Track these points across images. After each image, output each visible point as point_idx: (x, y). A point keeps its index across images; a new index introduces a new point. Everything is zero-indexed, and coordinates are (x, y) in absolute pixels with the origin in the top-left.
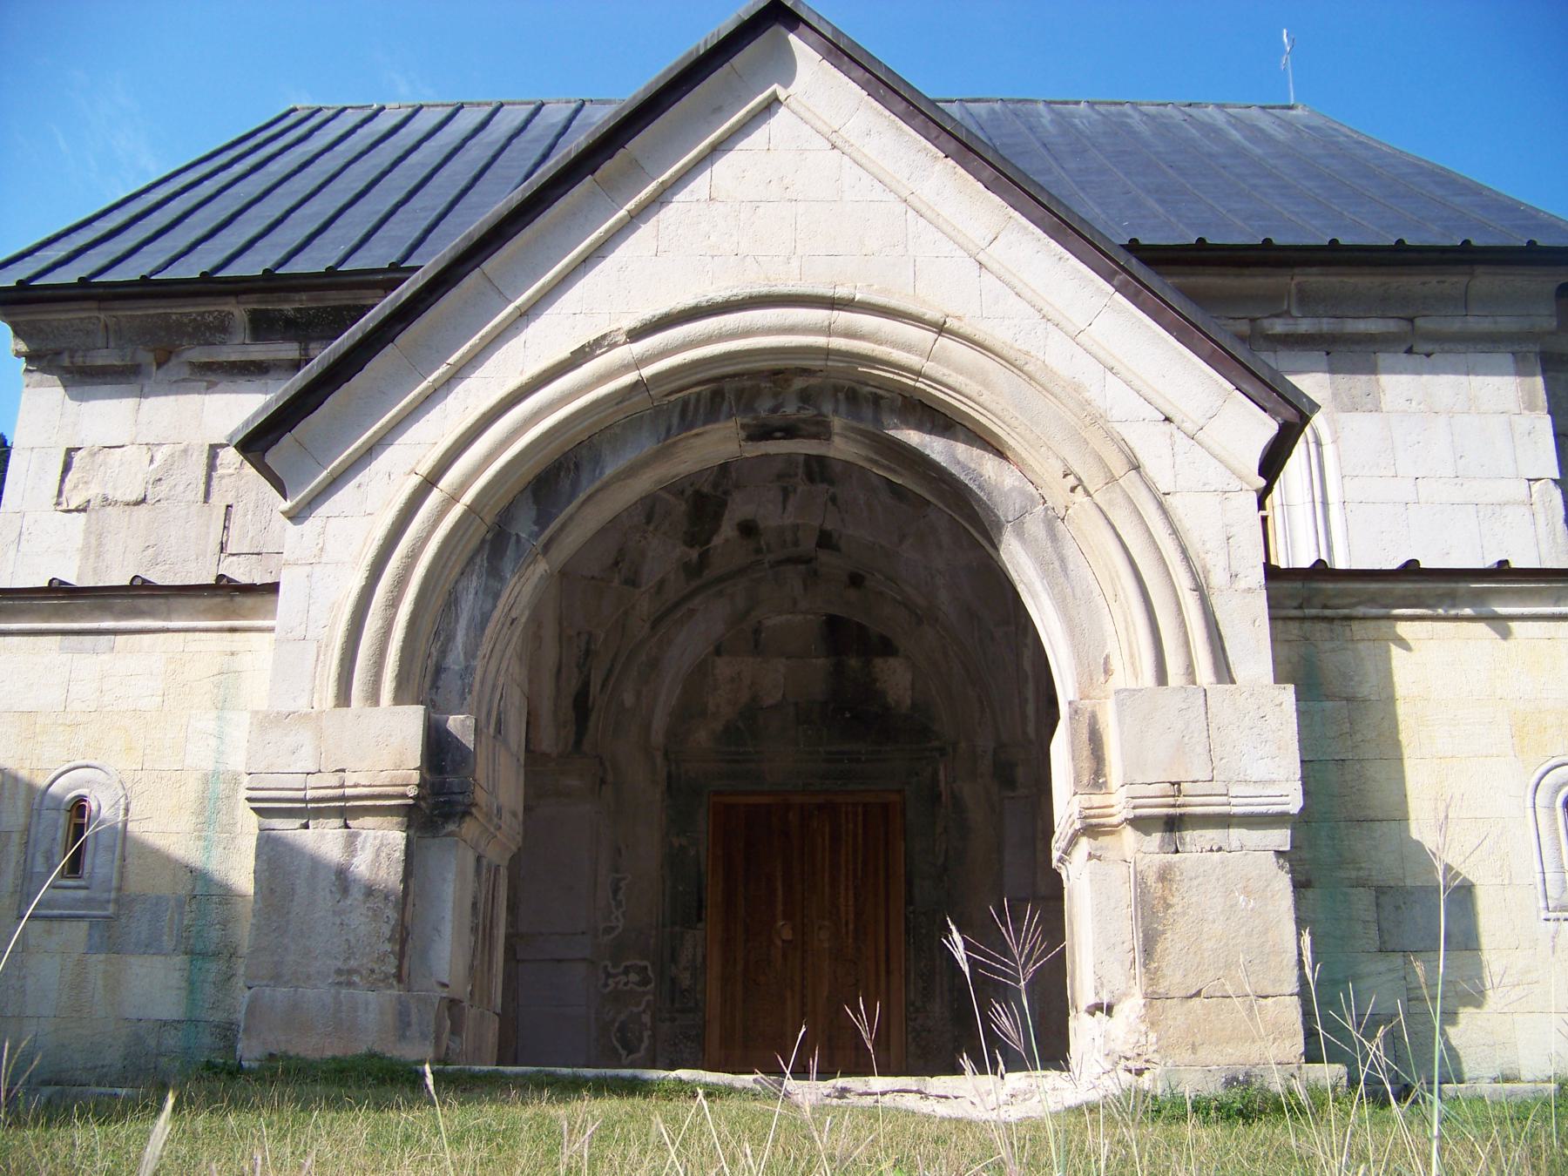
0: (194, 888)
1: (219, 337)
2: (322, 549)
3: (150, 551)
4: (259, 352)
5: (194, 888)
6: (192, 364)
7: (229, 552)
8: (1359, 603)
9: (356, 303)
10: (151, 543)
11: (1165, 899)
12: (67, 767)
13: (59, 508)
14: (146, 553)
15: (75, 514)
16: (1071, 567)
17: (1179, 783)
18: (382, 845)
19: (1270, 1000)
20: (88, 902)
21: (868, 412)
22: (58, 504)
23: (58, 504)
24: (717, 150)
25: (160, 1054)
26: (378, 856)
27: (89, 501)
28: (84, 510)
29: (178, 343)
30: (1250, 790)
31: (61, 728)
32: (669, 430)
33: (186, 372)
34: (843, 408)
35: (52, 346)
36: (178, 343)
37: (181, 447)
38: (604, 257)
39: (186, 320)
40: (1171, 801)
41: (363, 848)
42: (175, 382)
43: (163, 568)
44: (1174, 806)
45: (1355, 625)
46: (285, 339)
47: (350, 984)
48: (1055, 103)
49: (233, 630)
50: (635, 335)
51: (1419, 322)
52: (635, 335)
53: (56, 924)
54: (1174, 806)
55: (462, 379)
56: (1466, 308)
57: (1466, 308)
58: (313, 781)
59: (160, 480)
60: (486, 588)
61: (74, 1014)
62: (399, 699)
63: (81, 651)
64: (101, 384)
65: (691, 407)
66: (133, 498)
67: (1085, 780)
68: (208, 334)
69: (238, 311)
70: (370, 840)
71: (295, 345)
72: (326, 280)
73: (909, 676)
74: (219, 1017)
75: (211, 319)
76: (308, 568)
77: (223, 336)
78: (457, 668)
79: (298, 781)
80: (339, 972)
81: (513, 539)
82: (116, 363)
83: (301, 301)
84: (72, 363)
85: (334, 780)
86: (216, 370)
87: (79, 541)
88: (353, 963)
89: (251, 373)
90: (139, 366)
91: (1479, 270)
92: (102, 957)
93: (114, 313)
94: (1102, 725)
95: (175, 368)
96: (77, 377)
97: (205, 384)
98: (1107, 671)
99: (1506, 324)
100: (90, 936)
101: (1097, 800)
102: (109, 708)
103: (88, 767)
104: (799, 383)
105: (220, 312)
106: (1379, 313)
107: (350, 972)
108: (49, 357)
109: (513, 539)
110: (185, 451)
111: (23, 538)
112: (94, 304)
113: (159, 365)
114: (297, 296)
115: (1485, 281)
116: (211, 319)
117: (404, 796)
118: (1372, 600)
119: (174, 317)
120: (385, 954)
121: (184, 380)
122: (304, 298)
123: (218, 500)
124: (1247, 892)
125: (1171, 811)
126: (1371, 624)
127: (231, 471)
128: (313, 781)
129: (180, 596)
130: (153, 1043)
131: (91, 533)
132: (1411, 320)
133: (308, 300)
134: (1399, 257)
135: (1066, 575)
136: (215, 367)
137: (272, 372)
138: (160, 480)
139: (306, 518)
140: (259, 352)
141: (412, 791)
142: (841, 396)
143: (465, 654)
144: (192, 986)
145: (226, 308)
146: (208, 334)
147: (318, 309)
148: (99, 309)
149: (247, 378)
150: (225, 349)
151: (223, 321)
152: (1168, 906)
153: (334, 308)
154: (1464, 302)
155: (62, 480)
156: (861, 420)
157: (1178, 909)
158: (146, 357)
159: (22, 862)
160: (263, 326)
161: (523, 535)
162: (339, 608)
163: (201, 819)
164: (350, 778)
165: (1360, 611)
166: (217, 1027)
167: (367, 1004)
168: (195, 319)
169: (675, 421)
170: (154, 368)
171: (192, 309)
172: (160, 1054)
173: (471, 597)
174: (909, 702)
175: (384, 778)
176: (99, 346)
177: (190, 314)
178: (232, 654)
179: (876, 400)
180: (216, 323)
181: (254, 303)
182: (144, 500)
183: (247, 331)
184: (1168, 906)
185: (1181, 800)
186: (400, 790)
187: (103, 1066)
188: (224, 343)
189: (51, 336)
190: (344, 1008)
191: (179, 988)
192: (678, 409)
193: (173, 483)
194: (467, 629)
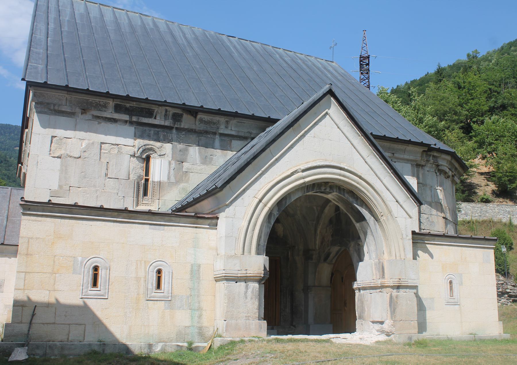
0: (191, 293)
1: (104, 109)
2: (235, 214)
3: (83, 174)
4: (116, 116)
5: (191, 293)
6: (93, 115)
7: (108, 177)
8: (419, 240)
9: (150, 108)
10: (84, 171)
11: (397, 302)
12: (155, 261)
13: (50, 155)
14: (81, 174)
15: (56, 158)
16: (378, 231)
17: (400, 279)
18: (254, 287)
19: (412, 322)
20: (164, 297)
21: (342, 192)
22: (50, 154)
23: (50, 154)
24: (316, 124)
25: (185, 334)
26: (253, 290)
27: (62, 155)
28: (60, 158)
29: (90, 108)
30: (411, 281)
31: (152, 250)
32: (304, 192)
33: (90, 117)
34: (338, 191)
35: (47, 101)
36: (90, 108)
37: (91, 142)
38: (293, 148)
39: (94, 102)
40: (399, 282)
41: (250, 288)
42: (87, 120)
43: (88, 179)
44: (399, 283)
45: (418, 244)
46: (125, 114)
47: (249, 319)
48: (286, 50)
49: (196, 227)
50: (303, 171)
51: (395, 155)
52: (303, 171)
53: (156, 302)
54: (399, 283)
55: (264, 174)
56: (405, 153)
57: (405, 153)
58: (240, 272)
59: (85, 151)
60: (268, 226)
61: (162, 325)
62: (258, 253)
63: (155, 229)
64: (62, 116)
65: (309, 187)
66: (77, 156)
67: (381, 277)
68: (100, 108)
69: (111, 103)
70: (251, 286)
71: (128, 116)
72: (144, 101)
73: (283, 228)
74: (199, 325)
75: (102, 103)
76: (232, 219)
77: (105, 109)
78: (262, 245)
79: (236, 272)
80: (246, 317)
81: (273, 215)
82: (69, 111)
83: (133, 104)
84: (54, 108)
85: (245, 272)
86: (100, 118)
87: (59, 167)
88: (249, 315)
89: (112, 121)
90: (75, 113)
91: (410, 145)
92: (168, 310)
93: (71, 96)
94: (384, 265)
95: (88, 116)
96: (53, 112)
97: (97, 122)
98: (384, 254)
99: (411, 158)
100: (165, 305)
101: (383, 280)
102: (165, 246)
103: (161, 261)
104: (330, 184)
105: (106, 102)
106: (388, 151)
107: (249, 316)
108: (45, 104)
109: (273, 215)
110: (93, 143)
111: (39, 163)
112: (66, 92)
113: (82, 114)
114: (132, 103)
115: (410, 148)
116: (102, 103)
117: (261, 277)
118: (421, 240)
119: (90, 100)
120: (256, 312)
121: (90, 120)
122: (134, 104)
123: (104, 160)
124: (409, 300)
125: (399, 284)
126: (420, 244)
127: (107, 152)
128: (240, 272)
129: (183, 217)
130: (184, 332)
131: (63, 165)
132: (393, 154)
133: (135, 104)
134: (397, 140)
135: (377, 233)
136: (100, 117)
137: (118, 122)
138: (85, 151)
139: (230, 206)
140: (116, 116)
141: (262, 276)
142: (337, 188)
143: (264, 241)
144: (192, 318)
145: (109, 102)
146: (100, 108)
147: (136, 107)
148: (67, 94)
149: (111, 123)
150: (105, 113)
151: (106, 105)
152: (397, 303)
153: (142, 108)
154: (404, 151)
155: (51, 146)
156: (341, 194)
157: (399, 304)
158: (78, 110)
159: (145, 285)
160: (118, 109)
161: (275, 214)
162: (241, 229)
163: (192, 276)
164: (249, 272)
165: (419, 241)
166: (199, 327)
167: (252, 324)
168: (97, 102)
169: (306, 190)
170: (80, 114)
171: (97, 100)
172: (185, 334)
173: (265, 227)
174: (282, 235)
175: (256, 272)
176: (63, 104)
177: (96, 101)
178: (197, 234)
179: (344, 189)
180: (103, 104)
181: (118, 102)
182: (80, 157)
183: (113, 109)
184: (397, 303)
185: (401, 282)
186: (260, 275)
187: (171, 338)
188: (105, 111)
189: (47, 98)
190: (248, 325)
191: (189, 318)
192: (306, 188)
193: (89, 153)
194: (264, 235)
